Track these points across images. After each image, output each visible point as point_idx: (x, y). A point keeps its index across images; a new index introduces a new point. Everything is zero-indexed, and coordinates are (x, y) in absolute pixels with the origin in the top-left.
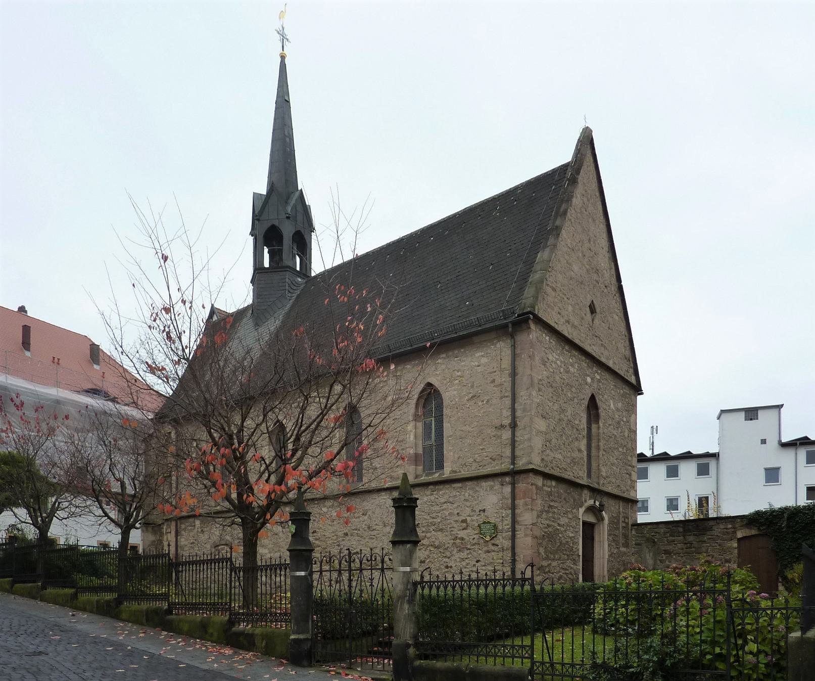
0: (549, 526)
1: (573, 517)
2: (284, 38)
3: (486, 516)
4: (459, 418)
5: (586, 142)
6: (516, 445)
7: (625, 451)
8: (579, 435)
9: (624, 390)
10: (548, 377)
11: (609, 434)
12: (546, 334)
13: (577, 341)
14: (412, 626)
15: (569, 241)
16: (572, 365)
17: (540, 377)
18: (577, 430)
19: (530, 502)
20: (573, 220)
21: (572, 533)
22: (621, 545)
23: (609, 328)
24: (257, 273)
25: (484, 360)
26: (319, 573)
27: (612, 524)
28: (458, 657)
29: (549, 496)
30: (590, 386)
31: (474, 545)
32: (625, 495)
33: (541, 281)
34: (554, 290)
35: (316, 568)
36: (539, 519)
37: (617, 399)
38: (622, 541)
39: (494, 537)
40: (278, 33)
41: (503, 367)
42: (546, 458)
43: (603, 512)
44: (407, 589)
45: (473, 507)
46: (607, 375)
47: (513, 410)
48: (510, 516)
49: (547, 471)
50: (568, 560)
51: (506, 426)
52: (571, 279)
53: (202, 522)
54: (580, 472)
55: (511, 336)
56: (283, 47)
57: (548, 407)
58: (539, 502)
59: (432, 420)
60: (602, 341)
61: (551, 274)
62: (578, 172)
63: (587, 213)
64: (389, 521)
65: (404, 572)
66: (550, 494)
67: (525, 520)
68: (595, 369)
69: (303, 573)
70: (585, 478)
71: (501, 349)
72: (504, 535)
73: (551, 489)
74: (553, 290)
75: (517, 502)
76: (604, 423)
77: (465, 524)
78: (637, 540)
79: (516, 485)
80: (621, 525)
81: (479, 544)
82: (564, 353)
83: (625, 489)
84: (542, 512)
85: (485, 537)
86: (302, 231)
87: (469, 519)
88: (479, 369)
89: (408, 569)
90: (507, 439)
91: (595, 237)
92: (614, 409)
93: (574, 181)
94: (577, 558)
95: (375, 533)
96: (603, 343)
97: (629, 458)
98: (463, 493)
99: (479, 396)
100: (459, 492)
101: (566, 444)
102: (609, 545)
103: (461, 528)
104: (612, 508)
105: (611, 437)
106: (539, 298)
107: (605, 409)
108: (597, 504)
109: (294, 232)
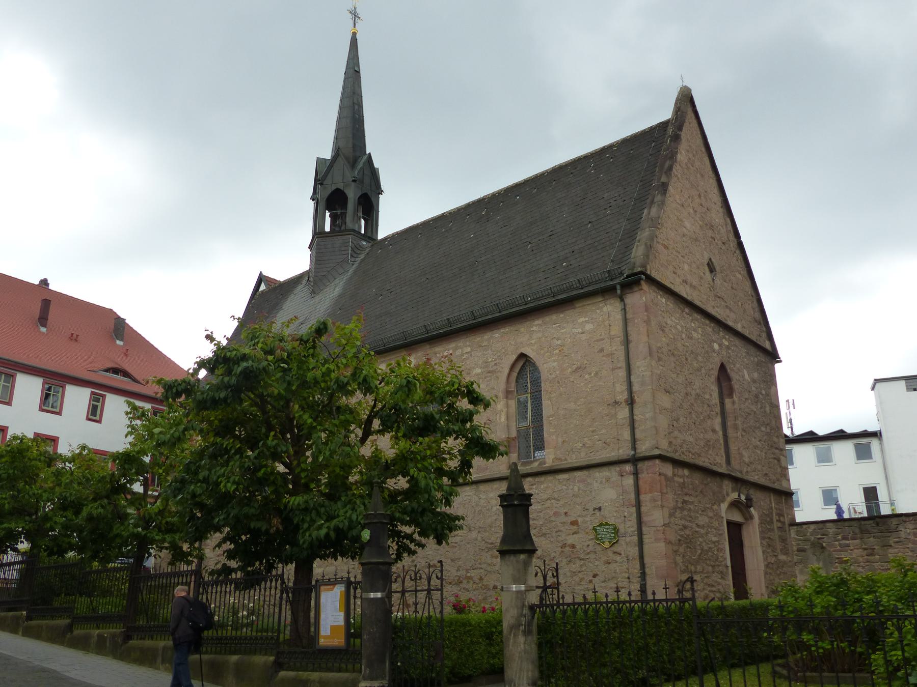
0: (685, 527)
1: (715, 515)
2: (355, 15)
4: (561, 394)
6: (636, 426)
10: (668, 345)
11: (747, 410)
13: (698, 303)
14: (530, 667)
15: (677, 197)
16: (695, 330)
17: (659, 345)
18: (709, 406)
20: (679, 176)
21: (715, 536)
22: (779, 551)
24: (317, 237)
25: (589, 327)
27: (764, 524)
29: (682, 488)
31: (588, 554)
32: (776, 486)
33: (652, 238)
34: (666, 247)
36: (672, 519)
38: (779, 545)
39: (614, 543)
40: (351, 13)
41: (613, 333)
42: (674, 442)
43: (752, 509)
46: (737, 341)
47: (630, 384)
49: (676, 456)
50: (713, 572)
51: (621, 403)
52: (684, 235)
56: (355, 24)
57: (671, 380)
58: (670, 496)
59: (527, 397)
60: (726, 302)
62: (680, 128)
63: (695, 169)
65: (518, 592)
66: (683, 486)
69: (379, 595)
70: (724, 465)
72: (628, 539)
73: (684, 481)
74: (665, 248)
75: (642, 497)
77: (575, 527)
78: (798, 544)
79: (639, 476)
80: (776, 525)
81: (595, 552)
82: (683, 316)
84: (675, 508)
85: (603, 543)
86: (369, 194)
87: (580, 520)
88: (584, 337)
89: (523, 587)
91: (706, 192)
93: (676, 138)
94: (725, 570)
96: (728, 304)
97: (775, 439)
98: (571, 487)
99: (585, 368)
101: (697, 423)
102: (763, 552)
103: (571, 532)
104: (762, 503)
105: (749, 414)
106: (650, 257)
108: (743, 497)
109: (360, 194)
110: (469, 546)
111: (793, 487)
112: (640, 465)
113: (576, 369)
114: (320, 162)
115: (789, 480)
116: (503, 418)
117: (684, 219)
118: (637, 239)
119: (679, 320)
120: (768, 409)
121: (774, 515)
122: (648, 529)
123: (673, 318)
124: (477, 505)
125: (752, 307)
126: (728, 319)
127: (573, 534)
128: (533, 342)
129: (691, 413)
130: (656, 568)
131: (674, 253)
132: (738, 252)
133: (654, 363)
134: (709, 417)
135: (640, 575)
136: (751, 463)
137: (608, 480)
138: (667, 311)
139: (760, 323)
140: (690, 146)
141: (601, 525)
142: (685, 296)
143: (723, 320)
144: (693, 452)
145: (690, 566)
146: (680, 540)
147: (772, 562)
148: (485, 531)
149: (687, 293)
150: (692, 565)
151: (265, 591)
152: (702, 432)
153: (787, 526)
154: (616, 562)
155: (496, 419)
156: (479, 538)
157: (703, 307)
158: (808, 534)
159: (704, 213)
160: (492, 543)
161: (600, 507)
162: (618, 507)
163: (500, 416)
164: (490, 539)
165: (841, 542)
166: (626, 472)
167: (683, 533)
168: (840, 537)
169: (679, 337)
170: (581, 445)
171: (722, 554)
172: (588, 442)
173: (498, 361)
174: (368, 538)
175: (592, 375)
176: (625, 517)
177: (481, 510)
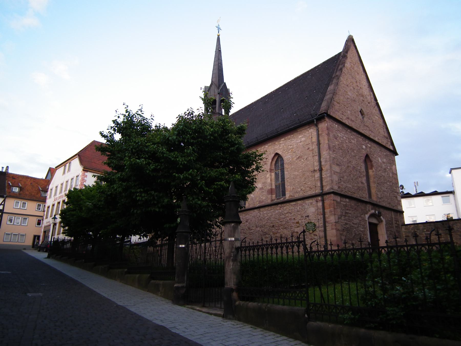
0: (346, 224)
2: (219, 29)
3: (309, 219)
4: (292, 169)
5: (350, 42)
6: (323, 180)
7: (391, 184)
11: (380, 175)
12: (335, 124)
13: (355, 128)
16: (353, 139)
17: (334, 145)
18: (360, 172)
19: (333, 210)
20: (346, 73)
21: (362, 228)
23: (373, 122)
25: (303, 139)
30: (365, 150)
32: (395, 208)
33: (332, 99)
34: (338, 103)
36: (340, 220)
39: (314, 231)
40: (217, 27)
41: (313, 141)
42: (341, 186)
43: (381, 217)
44: (232, 252)
45: (302, 215)
46: (375, 145)
47: (320, 162)
48: (322, 218)
49: (342, 193)
52: (348, 99)
54: (364, 195)
55: (316, 125)
56: (219, 32)
58: (339, 210)
61: (336, 96)
66: (345, 206)
67: (331, 220)
68: (367, 142)
69: (183, 246)
70: (368, 198)
71: (311, 132)
72: (320, 229)
74: (338, 103)
75: (326, 211)
76: (376, 169)
77: (298, 224)
78: (406, 234)
80: (394, 225)
83: (394, 205)
84: (341, 216)
87: (300, 221)
89: (233, 239)
92: (381, 162)
95: (252, 231)
96: (371, 129)
99: (302, 157)
101: (353, 179)
103: (296, 226)
104: (387, 215)
107: (376, 162)
108: (377, 212)
111: (403, 210)
112: (325, 197)
113: (298, 157)
115: (402, 206)
117: (348, 92)
118: (324, 99)
119: (344, 134)
120: (391, 175)
121: (394, 221)
122: (329, 224)
123: (341, 133)
124: (259, 217)
125: (383, 131)
126: (370, 135)
127: (297, 227)
129: (350, 175)
131: (343, 106)
132: (376, 107)
133: (331, 152)
134: (360, 177)
136: (382, 198)
137: (311, 204)
138: (338, 130)
139: (387, 138)
140: (352, 61)
142: (348, 124)
143: (368, 136)
144: (351, 191)
147: (393, 241)
149: (349, 123)
150: (350, 240)
151: (164, 250)
152: (356, 183)
153: (400, 226)
156: (260, 230)
157: (357, 129)
158: (410, 229)
159: (359, 90)
160: (265, 232)
165: (426, 233)
166: (319, 200)
167: (345, 226)
168: (425, 230)
169: (345, 142)
171: (366, 237)
173: (267, 157)
176: (318, 219)
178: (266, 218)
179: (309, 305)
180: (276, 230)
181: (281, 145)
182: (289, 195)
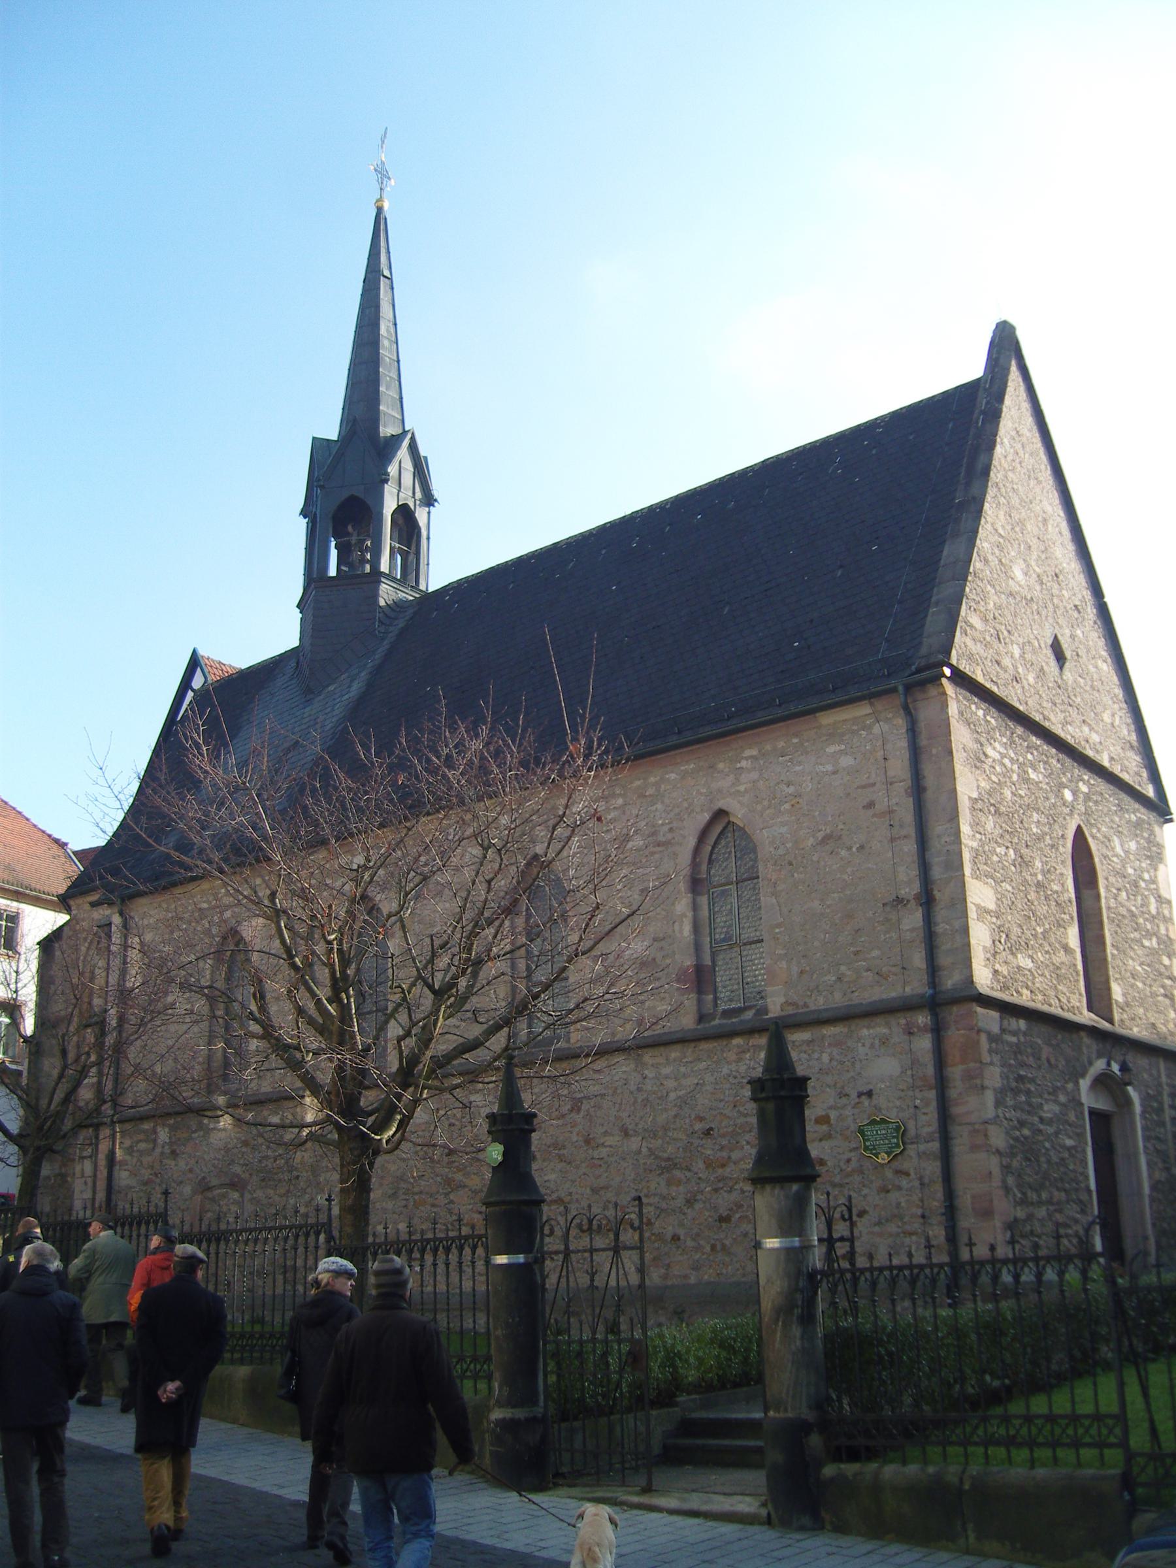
2: (382, 173)
3: (875, 1106)
8: (1063, 916)
9: (1139, 815)
21: (1070, 1137)
23: (1092, 687)
25: (846, 761)
26: (561, 1257)
28: (934, 1451)
29: (1015, 1053)
31: (848, 1175)
35: (552, 1244)
37: (1125, 832)
45: (843, 1087)
46: (1102, 785)
51: (908, 901)
53: (173, 1129)
64: (636, 1125)
72: (922, 1147)
77: (825, 1128)
87: (833, 1115)
90: (912, 930)
95: (604, 1152)
98: (816, 1055)
100: (805, 1052)
108: (1115, 1067)
110: (626, 1165)
114: (319, 447)
116: (687, 929)
124: (639, 1090)
127: (821, 1140)
128: (742, 788)
130: (973, 1197)
135: (943, 1210)
141: (873, 1122)
145: (1029, 1193)
146: (1012, 1147)
147: (1163, 1179)
148: (655, 1137)
154: (899, 1188)
155: (674, 931)
156: (644, 1150)
160: (669, 1159)
161: (871, 1090)
162: (903, 1091)
163: (681, 926)
164: (666, 1152)
166: (919, 1028)
170: (834, 978)
172: (849, 973)
173: (675, 824)
174: (500, 1158)
175: (854, 849)
177: (647, 1099)
178: (672, 1096)
179: (1130, 1457)
180: (722, 1148)
181: (744, 778)
182: (783, 1000)
